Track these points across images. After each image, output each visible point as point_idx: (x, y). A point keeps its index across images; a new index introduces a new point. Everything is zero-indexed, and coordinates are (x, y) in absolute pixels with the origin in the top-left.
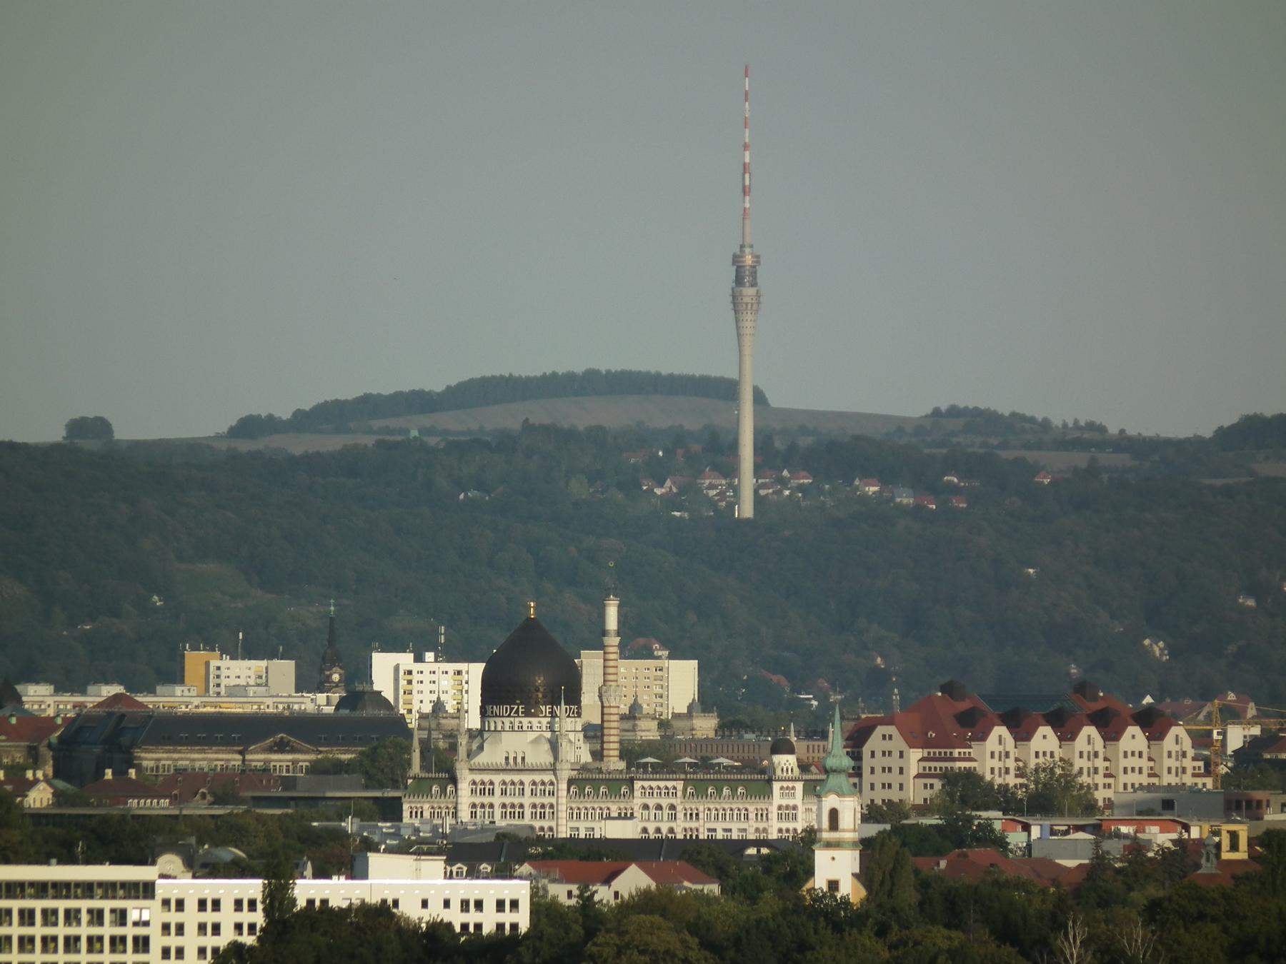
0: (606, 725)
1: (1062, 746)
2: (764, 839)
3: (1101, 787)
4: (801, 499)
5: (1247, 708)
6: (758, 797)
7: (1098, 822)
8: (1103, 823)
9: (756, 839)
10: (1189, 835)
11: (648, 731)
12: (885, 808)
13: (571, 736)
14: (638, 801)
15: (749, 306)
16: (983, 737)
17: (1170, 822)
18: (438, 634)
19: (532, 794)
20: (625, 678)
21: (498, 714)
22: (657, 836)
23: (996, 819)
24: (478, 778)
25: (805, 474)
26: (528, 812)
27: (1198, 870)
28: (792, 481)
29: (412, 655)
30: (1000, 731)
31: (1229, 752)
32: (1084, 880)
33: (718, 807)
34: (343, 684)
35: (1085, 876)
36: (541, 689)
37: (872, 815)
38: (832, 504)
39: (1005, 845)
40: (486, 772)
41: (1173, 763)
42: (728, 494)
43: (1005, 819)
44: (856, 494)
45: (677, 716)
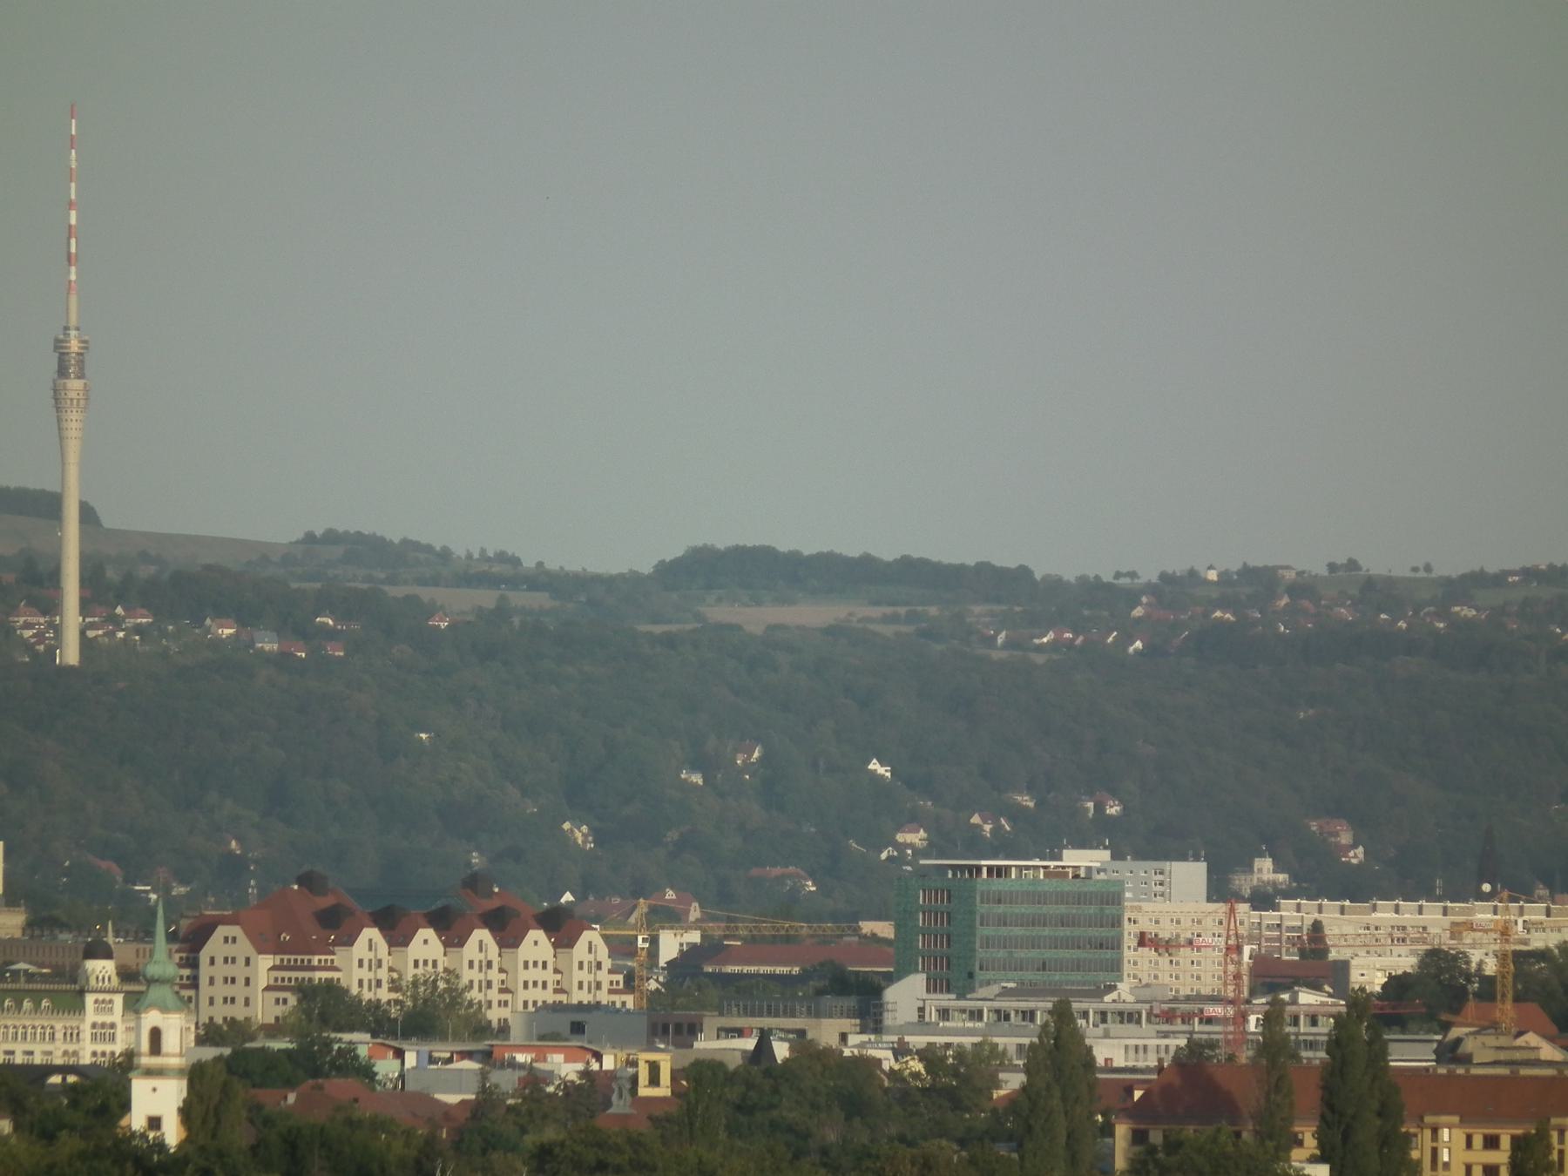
3: (495, 1004)
4: (138, 643)
5: (690, 910)
10: (601, 1066)
12: (225, 1028)
15: (75, 401)
16: (350, 941)
23: (362, 1043)
25: (145, 612)
27: (607, 1109)
30: (371, 933)
31: (662, 963)
32: (467, 1119)
35: (468, 1115)
38: (177, 650)
41: (585, 976)
42: (47, 635)
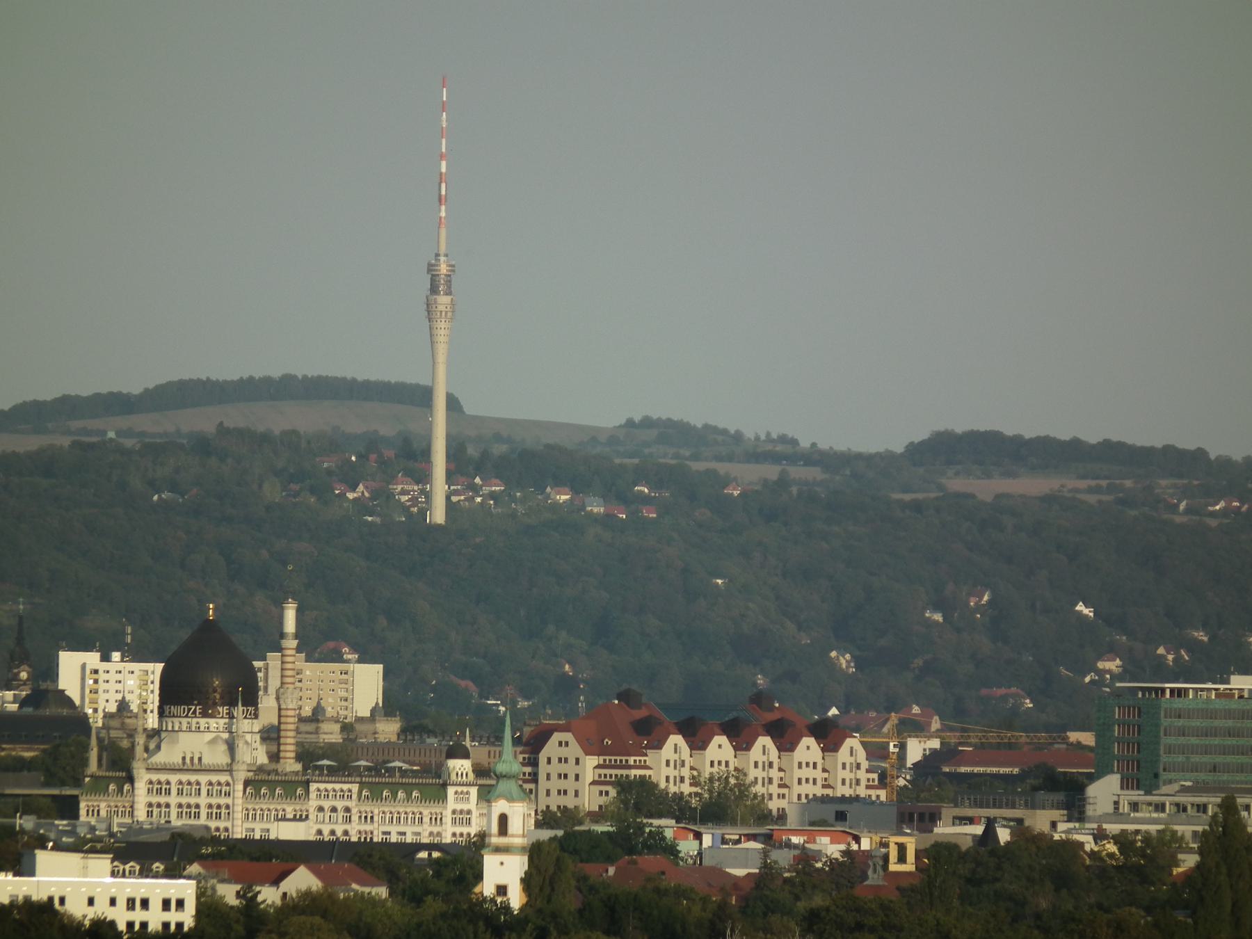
0: (283, 727)
1: (693, 755)
2: (416, 843)
3: (775, 797)
6: (375, 800)
7: (768, 831)
8: (775, 833)
9: (430, 843)
10: (860, 847)
11: (331, 734)
12: (559, 814)
13: (248, 737)
14: (313, 803)
15: (444, 314)
17: (842, 834)
18: (124, 634)
19: (208, 794)
20: (311, 681)
21: (176, 714)
22: (332, 838)
23: (668, 827)
24: (155, 777)
25: (498, 481)
26: (204, 812)
28: (484, 488)
29: (98, 654)
30: (676, 739)
31: (909, 765)
33: (393, 810)
34: (30, 683)
35: (753, 885)
36: (219, 690)
37: (547, 821)
39: (675, 853)
40: (162, 771)
41: (847, 774)
42: (420, 500)
43: (677, 827)
44: (547, 502)
45: (360, 720)
